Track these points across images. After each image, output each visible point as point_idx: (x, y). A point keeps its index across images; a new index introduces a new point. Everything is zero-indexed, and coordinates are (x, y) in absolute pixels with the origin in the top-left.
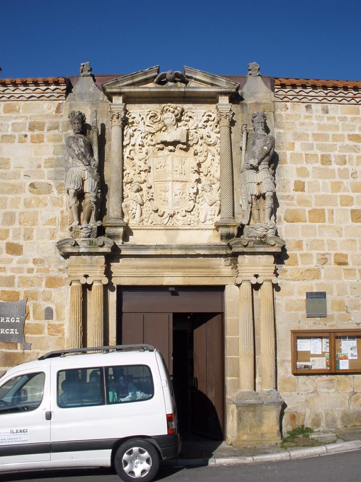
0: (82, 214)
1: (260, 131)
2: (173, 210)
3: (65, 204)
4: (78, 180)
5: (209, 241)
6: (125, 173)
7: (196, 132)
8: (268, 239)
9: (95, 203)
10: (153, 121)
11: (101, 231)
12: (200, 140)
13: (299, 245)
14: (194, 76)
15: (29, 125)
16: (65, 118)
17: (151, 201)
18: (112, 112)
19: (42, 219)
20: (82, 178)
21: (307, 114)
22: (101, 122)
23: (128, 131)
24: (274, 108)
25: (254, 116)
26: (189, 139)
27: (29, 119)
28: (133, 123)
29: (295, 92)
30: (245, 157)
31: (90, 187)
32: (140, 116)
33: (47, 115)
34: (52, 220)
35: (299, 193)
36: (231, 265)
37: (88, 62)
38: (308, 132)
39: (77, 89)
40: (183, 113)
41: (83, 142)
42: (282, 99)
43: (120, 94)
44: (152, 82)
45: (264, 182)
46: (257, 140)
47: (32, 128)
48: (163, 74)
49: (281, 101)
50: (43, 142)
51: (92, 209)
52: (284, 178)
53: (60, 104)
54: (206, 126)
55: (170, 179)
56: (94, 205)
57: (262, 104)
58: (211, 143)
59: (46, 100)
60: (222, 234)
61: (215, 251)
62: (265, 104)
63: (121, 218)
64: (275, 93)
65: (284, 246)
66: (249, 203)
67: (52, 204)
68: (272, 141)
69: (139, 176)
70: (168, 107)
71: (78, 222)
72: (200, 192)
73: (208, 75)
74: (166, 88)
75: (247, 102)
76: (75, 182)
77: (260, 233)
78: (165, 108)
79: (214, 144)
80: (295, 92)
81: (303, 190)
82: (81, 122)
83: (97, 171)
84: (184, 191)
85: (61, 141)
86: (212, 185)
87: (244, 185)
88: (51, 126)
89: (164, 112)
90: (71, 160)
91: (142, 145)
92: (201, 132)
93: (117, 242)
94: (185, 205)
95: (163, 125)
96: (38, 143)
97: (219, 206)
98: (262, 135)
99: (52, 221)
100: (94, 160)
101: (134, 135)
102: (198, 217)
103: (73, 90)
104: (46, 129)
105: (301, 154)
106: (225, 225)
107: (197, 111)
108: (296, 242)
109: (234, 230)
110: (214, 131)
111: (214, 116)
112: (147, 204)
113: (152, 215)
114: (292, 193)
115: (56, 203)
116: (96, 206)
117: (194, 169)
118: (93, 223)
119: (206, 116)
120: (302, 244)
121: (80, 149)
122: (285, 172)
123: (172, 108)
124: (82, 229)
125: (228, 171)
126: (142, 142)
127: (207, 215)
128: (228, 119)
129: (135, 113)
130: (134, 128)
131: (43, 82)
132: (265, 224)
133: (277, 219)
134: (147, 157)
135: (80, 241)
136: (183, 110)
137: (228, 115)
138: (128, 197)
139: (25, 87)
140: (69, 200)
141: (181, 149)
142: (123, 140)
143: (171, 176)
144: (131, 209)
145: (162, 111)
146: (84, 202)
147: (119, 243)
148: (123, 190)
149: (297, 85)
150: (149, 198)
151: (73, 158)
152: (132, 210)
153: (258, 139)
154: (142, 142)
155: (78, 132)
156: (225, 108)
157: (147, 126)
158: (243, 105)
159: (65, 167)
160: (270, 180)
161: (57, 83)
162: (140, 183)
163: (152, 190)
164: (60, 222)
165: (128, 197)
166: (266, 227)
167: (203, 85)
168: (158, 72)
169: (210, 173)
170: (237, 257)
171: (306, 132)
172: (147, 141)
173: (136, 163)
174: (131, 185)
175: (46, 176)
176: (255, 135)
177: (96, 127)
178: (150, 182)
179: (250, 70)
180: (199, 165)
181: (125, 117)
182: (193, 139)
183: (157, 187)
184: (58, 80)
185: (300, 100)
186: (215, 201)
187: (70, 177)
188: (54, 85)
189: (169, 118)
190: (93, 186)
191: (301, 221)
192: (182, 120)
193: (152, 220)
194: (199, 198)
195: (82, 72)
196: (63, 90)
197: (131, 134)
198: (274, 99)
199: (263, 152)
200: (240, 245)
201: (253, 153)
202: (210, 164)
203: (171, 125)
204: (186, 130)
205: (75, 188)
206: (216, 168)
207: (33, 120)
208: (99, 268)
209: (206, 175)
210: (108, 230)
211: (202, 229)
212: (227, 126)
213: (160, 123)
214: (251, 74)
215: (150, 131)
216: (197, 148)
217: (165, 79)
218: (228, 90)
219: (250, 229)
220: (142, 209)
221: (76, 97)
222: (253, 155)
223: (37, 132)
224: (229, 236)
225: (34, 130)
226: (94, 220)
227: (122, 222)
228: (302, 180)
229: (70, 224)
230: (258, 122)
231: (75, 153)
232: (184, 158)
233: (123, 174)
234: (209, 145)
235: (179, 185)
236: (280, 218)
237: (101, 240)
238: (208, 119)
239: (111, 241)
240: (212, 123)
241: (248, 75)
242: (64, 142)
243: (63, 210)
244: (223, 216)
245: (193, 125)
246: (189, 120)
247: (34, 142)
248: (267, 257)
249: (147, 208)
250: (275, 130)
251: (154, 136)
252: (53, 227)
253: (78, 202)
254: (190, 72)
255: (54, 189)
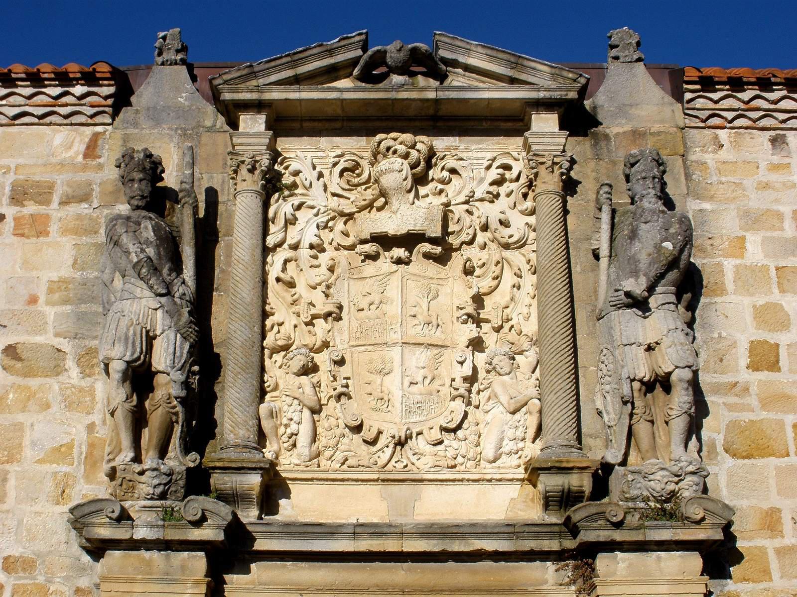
0: (146, 433)
1: (651, 203)
2: (405, 428)
3: (99, 406)
4: (135, 334)
5: (511, 515)
6: (268, 323)
7: (467, 211)
8: (683, 504)
9: (183, 401)
10: (348, 181)
11: (198, 481)
12: (479, 232)
13: (771, 522)
14: (462, 59)
15: (13, 190)
16: (108, 172)
17: (344, 399)
18: (237, 154)
19: (34, 444)
20: (148, 332)
21: (776, 159)
22: (205, 184)
23: (281, 207)
24: (685, 144)
25: (632, 161)
26: (450, 230)
27: (12, 174)
28: (294, 186)
29: (739, 99)
30: (609, 276)
31: (168, 355)
32: (314, 168)
33: (62, 164)
34: (63, 449)
35: (764, 375)
36: (575, 583)
37: (178, 30)
38: (781, 208)
39: (144, 95)
40: (434, 160)
41: (154, 231)
42: (704, 121)
43: (257, 106)
44: (350, 75)
45: (665, 342)
46: (643, 226)
47: (18, 196)
48: (379, 51)
49: (702, 125)
50: (47, 234)
51: (174, 418)
52: (720, 334)
53: (96, 136)
54: (497, 196)
55: (396, 337)
56: (179, 409)
57: (651, 134)
58: (511, 240)
59: (61, 125)
60: (547, 492)
61: (526, 542)
62: (659, 133)
63: (255, 446)
64: (686, 106)
65: (729, 524)
66: (625, 403)
67: (63, 405)
68: (684, 228)
69: (310, 332)
70: (391, 143)
71: (131, 455)
72: (482, 374)
73: (501, 55)
74: (385, 90)
75: (608, 131)
76: (127, 339)
77: (658, 487)
78: (383, 146)
79: (521, 244)
80: (739, 99)
81: (774, 366)
82: (149, 178)
83: (189, 312)
84: (435, 372)
85: (96, 233)
86: (515, 356)
87: (609, 354)
88: (70, 191)
89: (380, 157)
90: (118, 282)
91: (318, 245)
92: (482, 210)
93: (245, 514)
94: (438, 411)
95: (377, 192)
96: (33, 236)
97: (538, 415)
98: (654, 212)
99: (61, 453)
100: (184, 282)
101: (296, 219)
102: (478, 445)
103: (133, 99)
104: (56, 199)
105: (765, 268)
106: (557, 465)
107: (470, 154)
108: (761, 513)
109: (582, 480)
110: (519, 207)
111: (517, 167)
112: (332, 408)
113: (345, 441)
114: (745, 376)
115: (75, 402)
116: (184, 405)
117: (464, 311)
118: (176, 458)
119: (497, 168)
120: (781, 518)
121: (143, 250)
122: (722, 317)
123: (401, 143)
124: (142, 473)
125: (559, 316)
126: (319, 236)
127: (502, 440)
128: (557, 172)
129: (300, 159)
130: (296, 201)
131: (53, 76)
132: (673, 463)
133: (704, 448)
134: (334, 277)
135: (137, 508)
136: (431, 153)
137: (557, 163)
138: (276, 388)
139: (5, 87)
140: (110, 392)
141: (427, 256)
142: (265, 232)
143: (399, 330)
144: (285, 421)
145: (375, 155)
146: (152, 399)
147: (248, 517)
148: (263, 370)
149: (745, 80)
150: (337, 391)
151: (124, 276)
152: (286, 426)
153: (645, 223)
154: (319, 236)
155: (140, 204)
156: (549, 144)
157: (334, 195)
158: (596, 138)
159: (103, 303)
160: (680, 336)
161: (90, 79)
162: (311, 350)
163: (345, 371)
164: (84, 456)
165: (276, 388)
166: (675, 469)
167: (489, 83)
168: (365, 49)
169: (511, 323)
170: (594, 558)
171: (775, 207)
172: (331, 235)
173: (300, 296)
174: (286, 355)
175: (50, 329)
176: (635, 214)
177: (190, 192)
178: (340, 347)
179: (613, 47)
180: (478, 300)
181: (270, 169)
182: (461, 230)
183: (358, 361)
184: (94, 69)
185: (755, 121)
186: (526, 399)
187: (113, 326)
188: (82, 85)
189: (394, 171)
190: (178, 354)
191: (773, 455)
192: (430, 178)
193: (347, 453)
194: (478, 392)
195: (160, 54)
196: (106, 98)
197: (289, 216)
198: (681, 120)
199: (660, 255)
200: (602, 522)
201: (631, 261)
202: (508, 298)
203: (398, 189)
204: (442, 204)
205: (127, 358)
206: (525, 310)
207: (22, 177)
208: (191, 588)
209: (498, 330)
210: (218, 480)
211: (490, 480)
212: (556, 193)
213: (369, 188)
214: (616, 58)
215: (340, 208)
216: (473, 253)
217: (383, 69)
218: (557, 95)
219: (630, 477)
220: (317, 424)
221: (142, 119)
222: (633, 267)
223: (31, 208)
224: (565, 500)
225: (25, 203)
226: (178, 450)
227: (257, 456)
228: (772, 338)
229: (109, 461)
230: (644, 178)
231: (131, 261)
232: (435, 281)
233: (263, 326)
234: (506, 246)
235: (421, 357)
236: (713, 446)
237: (196, 505)
238: (503, 175)
239: (225, 510)
240: (514, 186)
241: (610, 60)
242: (102, 237)
243: (93, 424)
244: (551, 443)
245: (459, 193)
246: (450, 181)
247: (23, 235)
248: (680, 556)
249: (332, 420)
250: (688, 204)
251: (351, 222)
252: (64, 468)
253: (135, 397)
254: (452, 48)
255: (70, 363)
